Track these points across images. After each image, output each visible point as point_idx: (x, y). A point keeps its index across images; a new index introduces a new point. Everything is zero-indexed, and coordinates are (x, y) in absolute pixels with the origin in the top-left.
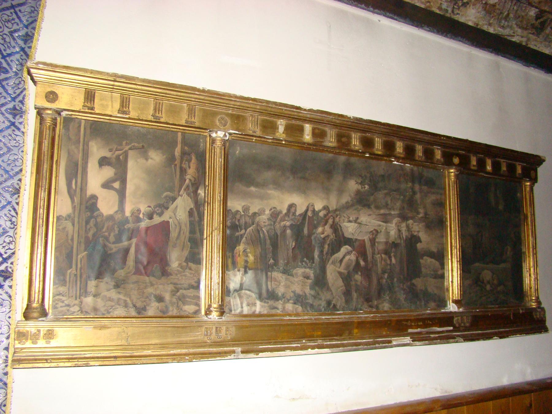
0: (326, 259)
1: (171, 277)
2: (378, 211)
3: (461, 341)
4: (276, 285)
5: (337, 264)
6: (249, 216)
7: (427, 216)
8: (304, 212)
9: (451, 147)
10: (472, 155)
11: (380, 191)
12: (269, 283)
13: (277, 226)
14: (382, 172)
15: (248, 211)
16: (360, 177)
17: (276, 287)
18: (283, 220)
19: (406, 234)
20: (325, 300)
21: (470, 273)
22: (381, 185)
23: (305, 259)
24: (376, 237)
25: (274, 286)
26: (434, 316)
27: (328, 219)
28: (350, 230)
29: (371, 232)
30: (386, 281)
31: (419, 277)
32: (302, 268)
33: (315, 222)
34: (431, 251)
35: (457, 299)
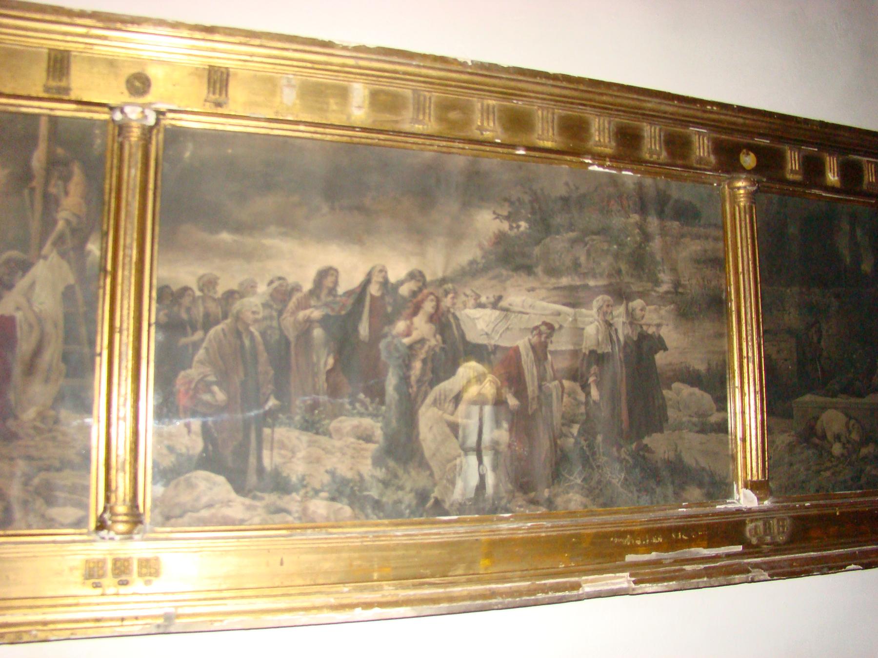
0: (417, 395)
1: (20, 442)
2: (553, 280)
3: (762, 578)
4: (284, 457)
5: (447, 405)
6: (214, 300)
7: (680, 290)
8: (360, 285)
9: (732, 129)
10: (787, 147)
11: (558, 232)
12: (266, 453)
13: (288, 320)
14: (562, 191)
15: (214, 288)
16: (507, 204)
17: (284, 463)
18: (303, 305)
19: (626, 332)
20: (411, 490)
21: (790, 416)
22: (559, 220)
23: (362, 396)
24: (549, 341)
25: (278, 460)
26: (693, 521)
27: (422, 301)
28: (481, 325)
29: (536, 328)
30: (577, 443)
31: (661, 430)
32: (353, 415)
33: (389, 309)
34: (691, 369)
35: (755, 479)
